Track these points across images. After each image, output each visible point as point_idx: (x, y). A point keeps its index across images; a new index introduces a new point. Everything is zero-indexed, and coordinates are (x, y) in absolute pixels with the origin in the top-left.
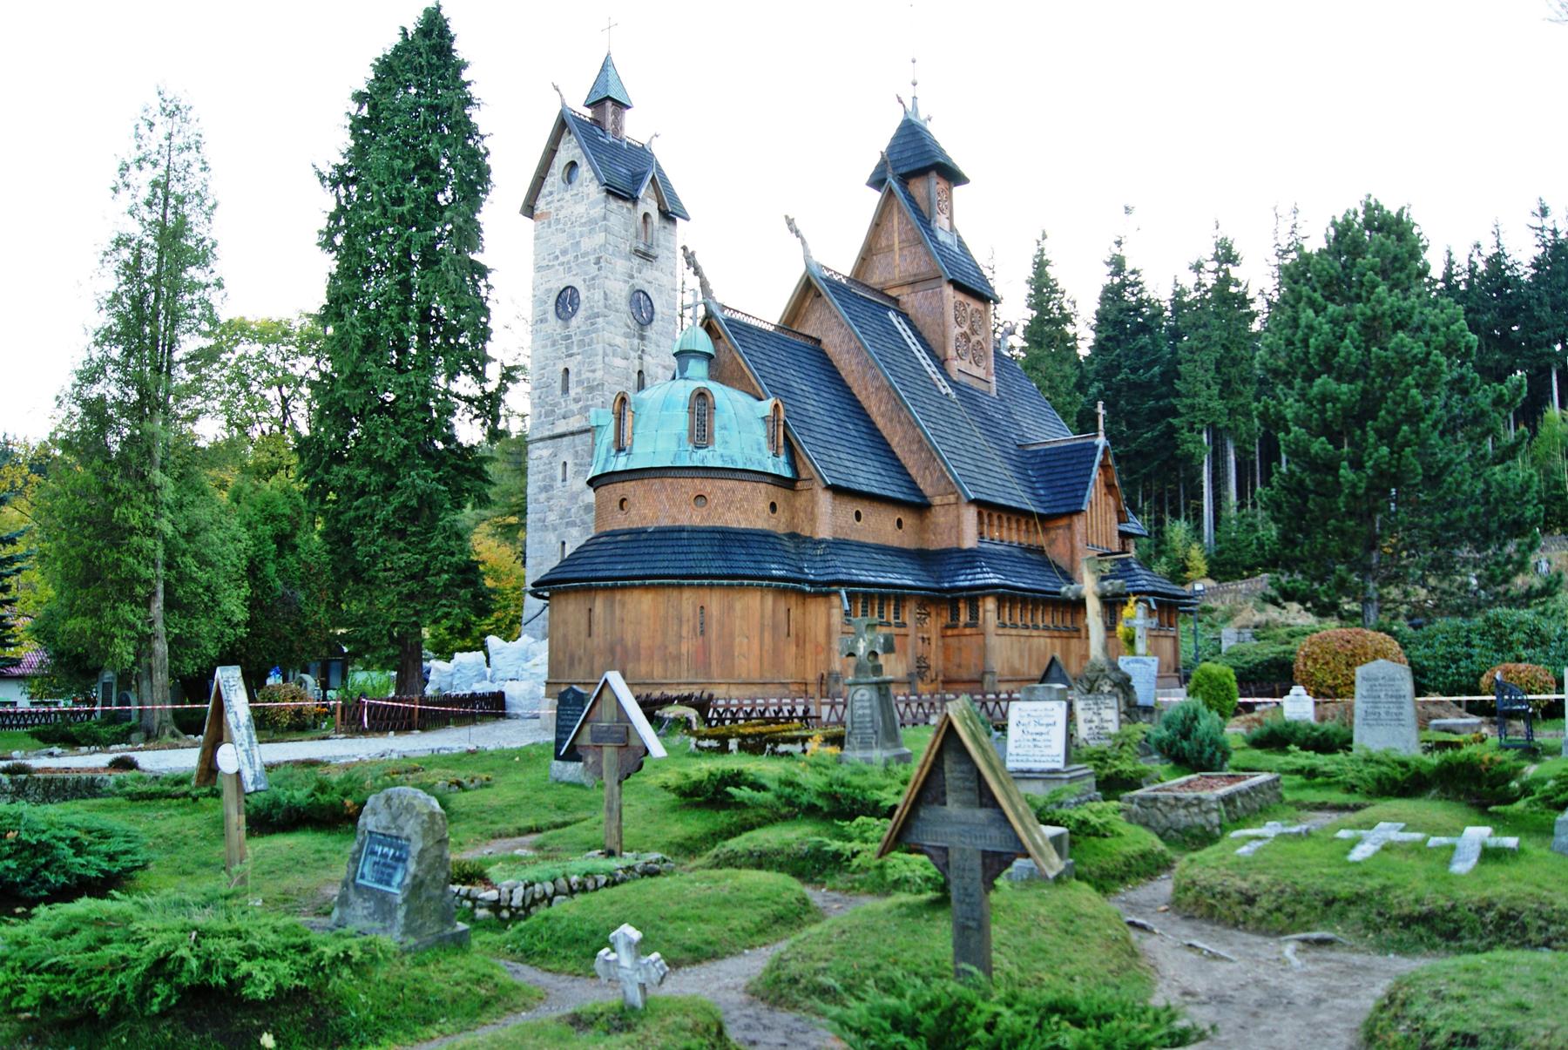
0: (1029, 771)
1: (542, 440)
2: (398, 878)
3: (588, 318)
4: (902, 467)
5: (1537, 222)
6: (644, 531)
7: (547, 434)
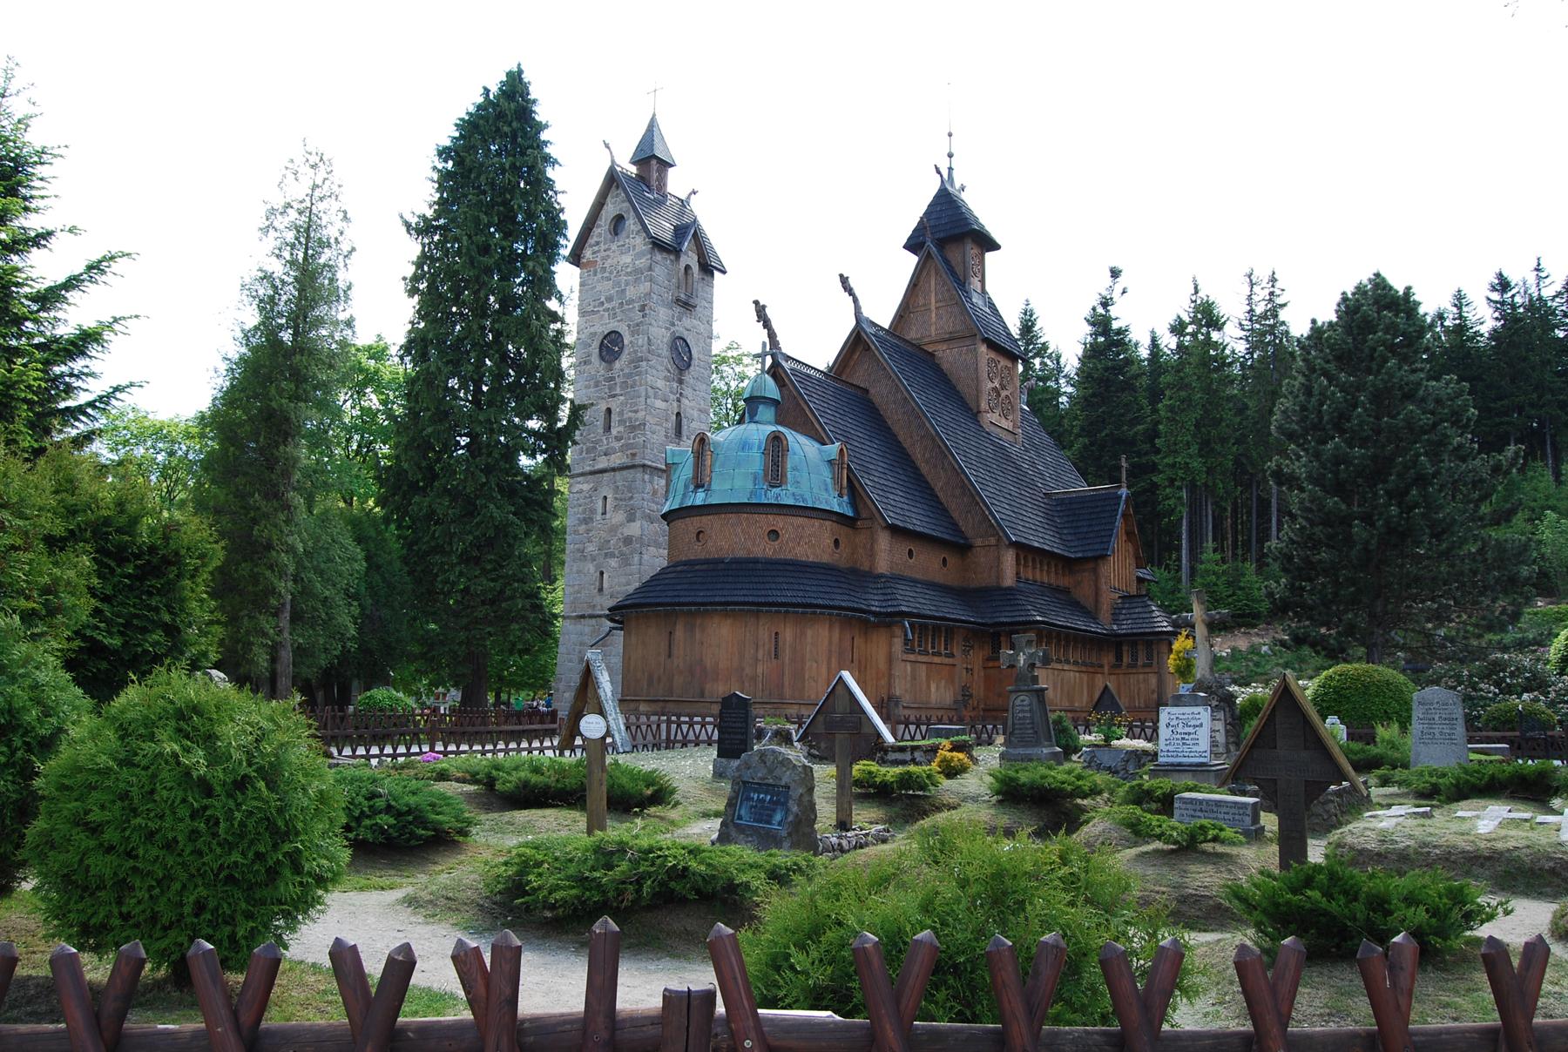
0: (1180, 764)
1: (582, 474)
2: (778, 817)
3: (631, 362)
4: (945, 510)
5: (1496, 296)
6: (721, 561)
7: (588, 469)
